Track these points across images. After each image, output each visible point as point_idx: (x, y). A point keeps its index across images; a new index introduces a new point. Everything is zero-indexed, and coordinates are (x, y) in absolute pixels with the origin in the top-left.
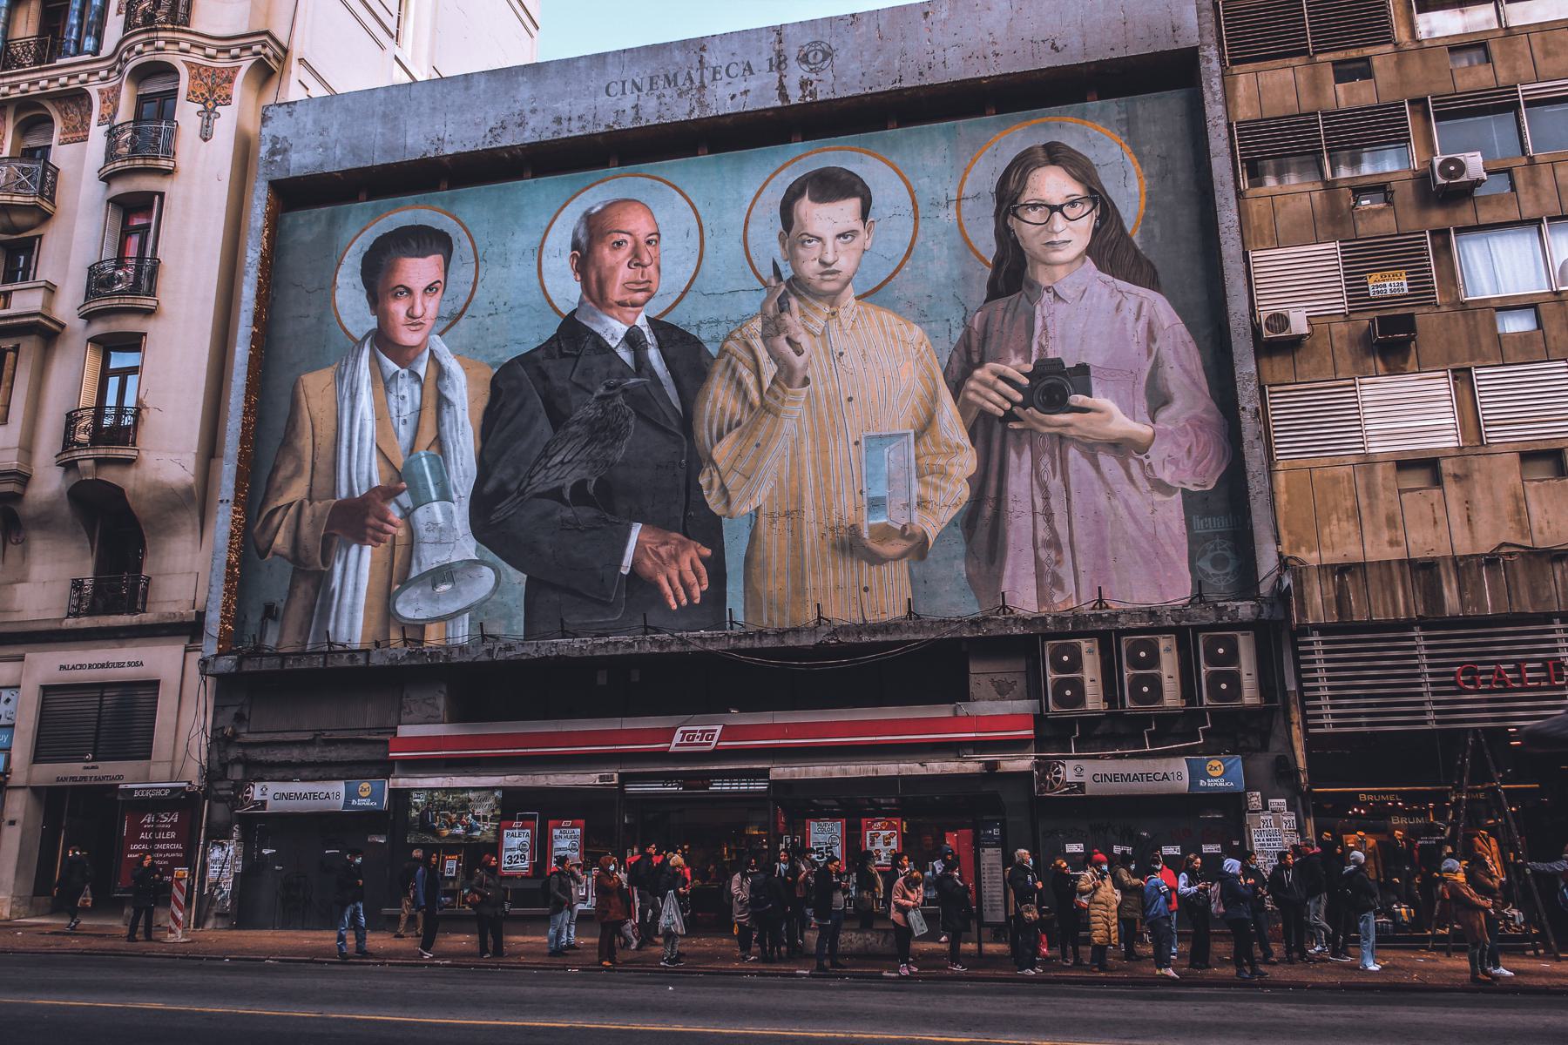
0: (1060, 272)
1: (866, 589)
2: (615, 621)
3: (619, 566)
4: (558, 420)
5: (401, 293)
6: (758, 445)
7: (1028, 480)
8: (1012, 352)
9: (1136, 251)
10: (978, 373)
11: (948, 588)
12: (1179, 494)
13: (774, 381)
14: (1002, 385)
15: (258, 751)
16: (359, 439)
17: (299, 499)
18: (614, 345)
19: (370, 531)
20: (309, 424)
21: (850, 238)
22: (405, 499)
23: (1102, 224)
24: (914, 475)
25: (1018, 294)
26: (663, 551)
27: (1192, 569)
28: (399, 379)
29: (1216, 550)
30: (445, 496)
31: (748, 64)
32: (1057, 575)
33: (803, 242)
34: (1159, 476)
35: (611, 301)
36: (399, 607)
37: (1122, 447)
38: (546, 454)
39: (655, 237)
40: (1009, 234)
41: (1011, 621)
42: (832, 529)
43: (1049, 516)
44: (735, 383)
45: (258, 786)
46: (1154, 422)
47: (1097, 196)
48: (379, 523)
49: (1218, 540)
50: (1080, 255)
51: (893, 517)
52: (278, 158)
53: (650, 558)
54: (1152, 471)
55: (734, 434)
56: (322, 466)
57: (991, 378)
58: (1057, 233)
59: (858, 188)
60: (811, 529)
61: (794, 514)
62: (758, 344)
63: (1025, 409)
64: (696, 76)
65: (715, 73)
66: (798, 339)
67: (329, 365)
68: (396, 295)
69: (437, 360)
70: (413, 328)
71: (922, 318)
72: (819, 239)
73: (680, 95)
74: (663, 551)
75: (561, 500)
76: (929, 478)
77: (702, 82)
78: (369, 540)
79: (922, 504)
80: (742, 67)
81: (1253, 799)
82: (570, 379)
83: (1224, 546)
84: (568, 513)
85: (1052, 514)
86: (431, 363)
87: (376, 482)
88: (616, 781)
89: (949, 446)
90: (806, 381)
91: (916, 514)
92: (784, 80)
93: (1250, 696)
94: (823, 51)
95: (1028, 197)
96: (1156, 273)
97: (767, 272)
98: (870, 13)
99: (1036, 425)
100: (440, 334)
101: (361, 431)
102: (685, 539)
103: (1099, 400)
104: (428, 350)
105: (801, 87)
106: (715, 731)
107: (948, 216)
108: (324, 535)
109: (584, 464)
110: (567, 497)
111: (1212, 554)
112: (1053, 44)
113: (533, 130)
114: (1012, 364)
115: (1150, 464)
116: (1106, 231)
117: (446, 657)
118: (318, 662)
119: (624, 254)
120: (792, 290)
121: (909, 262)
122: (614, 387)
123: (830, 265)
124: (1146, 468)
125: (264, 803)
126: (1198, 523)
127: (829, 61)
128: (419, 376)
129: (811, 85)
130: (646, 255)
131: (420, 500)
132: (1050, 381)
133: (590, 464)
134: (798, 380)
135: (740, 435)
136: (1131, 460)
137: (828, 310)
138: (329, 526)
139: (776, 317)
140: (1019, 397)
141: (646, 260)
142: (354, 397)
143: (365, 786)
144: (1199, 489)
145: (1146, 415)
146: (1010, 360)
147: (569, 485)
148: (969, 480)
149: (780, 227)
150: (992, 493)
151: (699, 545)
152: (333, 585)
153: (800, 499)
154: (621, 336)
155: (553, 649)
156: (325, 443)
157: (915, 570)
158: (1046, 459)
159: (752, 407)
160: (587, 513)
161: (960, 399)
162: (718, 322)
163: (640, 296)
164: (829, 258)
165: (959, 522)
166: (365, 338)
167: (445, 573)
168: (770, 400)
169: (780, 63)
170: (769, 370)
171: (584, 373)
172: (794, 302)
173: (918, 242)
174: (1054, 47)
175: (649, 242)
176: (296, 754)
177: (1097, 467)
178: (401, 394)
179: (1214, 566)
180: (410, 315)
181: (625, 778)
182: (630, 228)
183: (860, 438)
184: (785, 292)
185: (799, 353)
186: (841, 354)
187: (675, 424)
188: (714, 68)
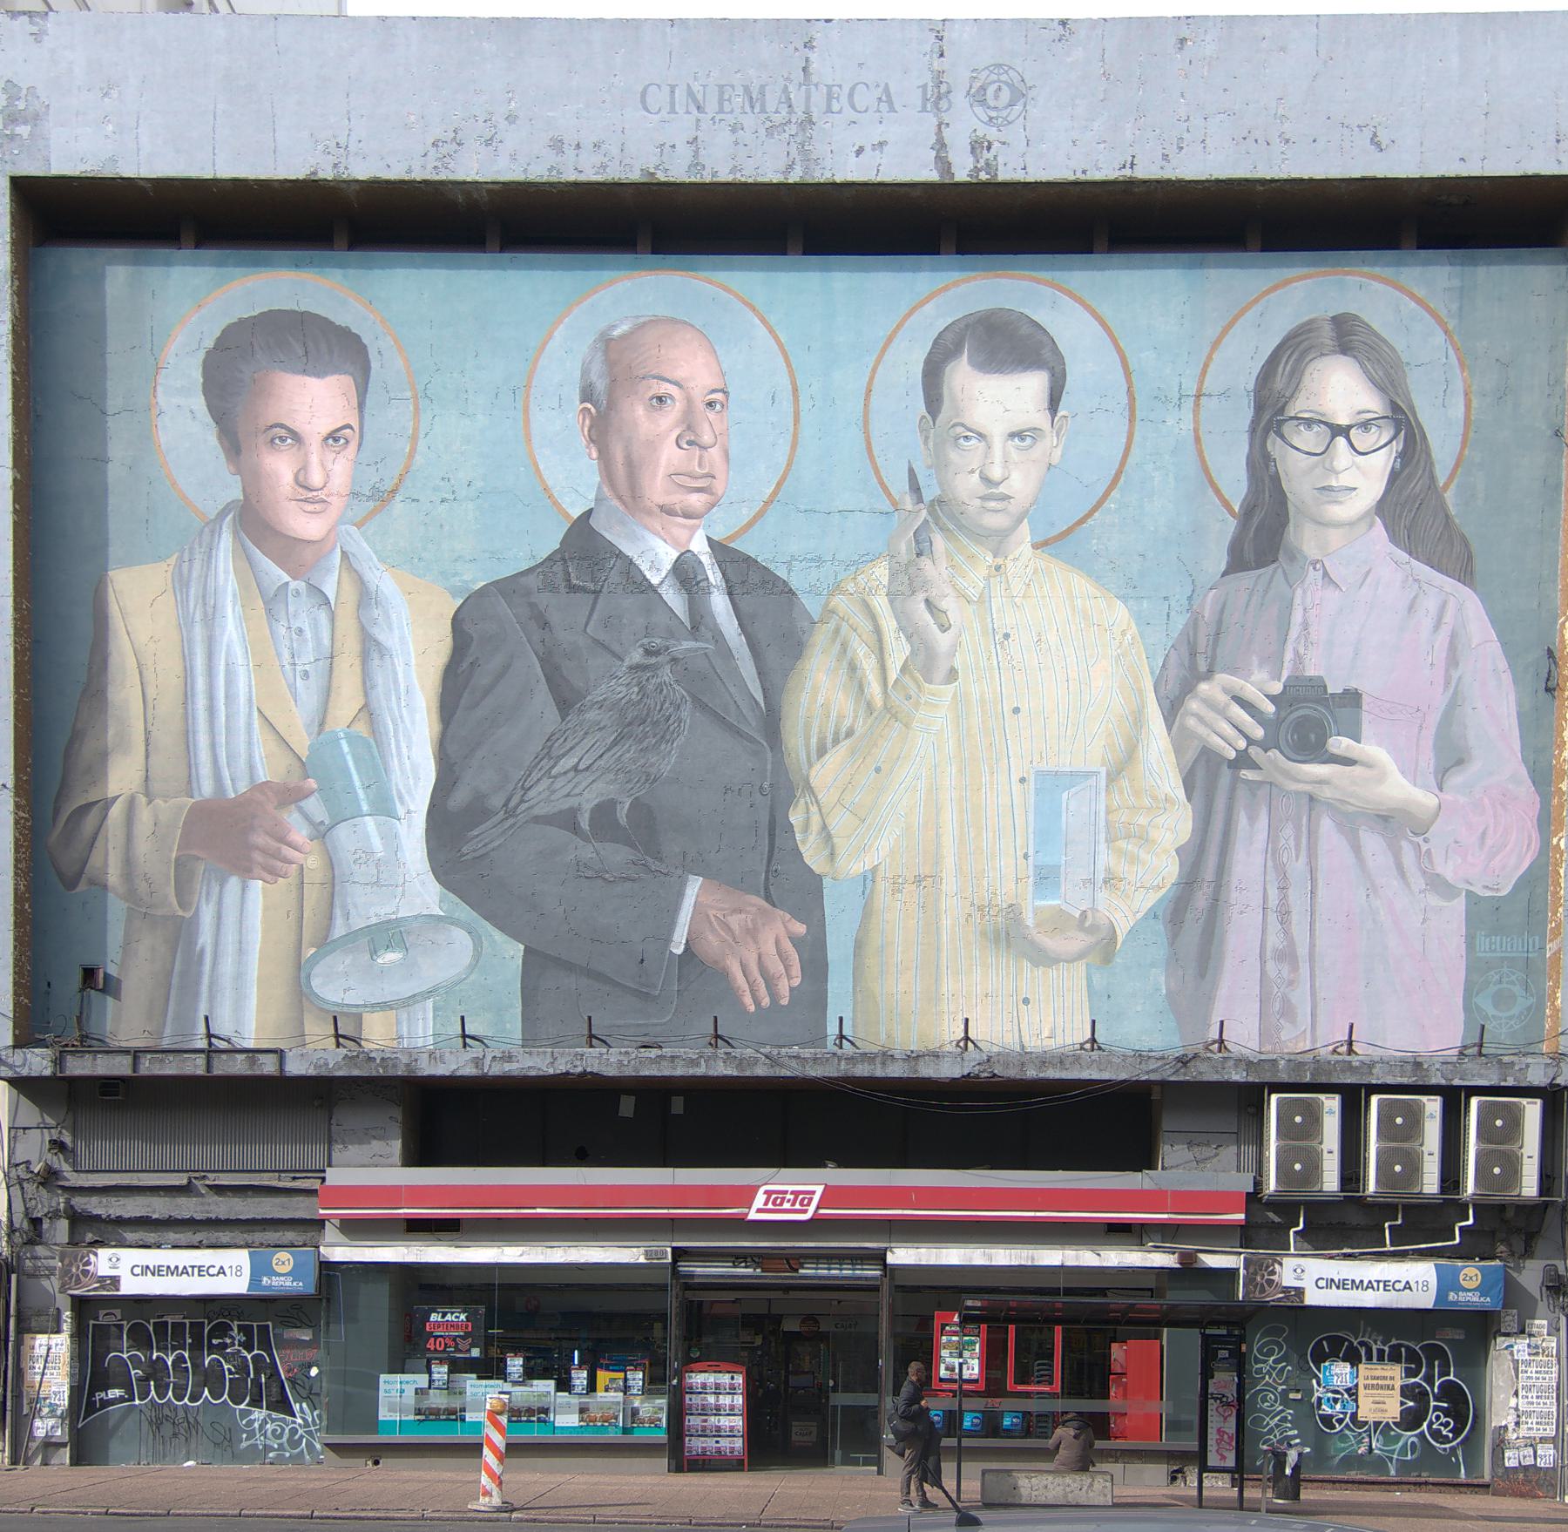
0: (1335, 537)
1: (1026, 1001)
2: (661, 1025)
3: (668, 940)
4: (566, 702)
5: (282, 439)
6: (878, 770)
7: (1259, 860)
8: (1255, 659)
9: (1447, 516)
10: (1203, 687)
11: (1139, 1009)
12: (1462, 898)
13: (904, 669)
14: (1237, 712)
15: (95, 1200)
16: (227, 697)
17: (127, 792)
18: (655, 581)
19: (258, 857)
20: (131, 662)
21: (1029, 441)
22: (313, 805)
23: (1403, 466)
24: (1102, 837)
25: (1274, 566)
26: (735, 921)
27: (1467, 1008)
28: (290, 598)
29: (1500, 982)
30: (384, 807)
31: (887, 90)
32: (1289, 1001)
33: (957, 439)
34: (1439, 870)
35: (649, 503)
36: (316, 983)
37: (1391, 821)
38: (548, 752)
39: (719, 396)
40: (1267, 466)
41: (1231, 1063)
42: (981, 908)
43: (1284, 914)
44: (845, 664)
45: (104, 1253)
46: (1441, 789)
47: (1402, 419)
48: (274, 844)
49: (1505, 970)
50: (1366, 515)
51: (1071, 898)
52: (23, 130)
53: (713, 930)
54: (1431, 862)
55: (845, 745)
56: (166, 738)
57: (1223, 698)
58: (1337, 473)
59: (1046, 353)
60: (952, 910)
61: (926, 880)
62: (881, 603)
63: (1266, 751)
64: (797, 97)
65: (830, 97)
66: (943, 605)
67: (160, 559)
68: (272, 441)
69: (356, 571)
70: (310, 508)
71: (1130, 591)
72: (981, 436)
73: (770, 132)
74: (735, 921)
75: (575, 829)
76: (1122, 844)
77: (807, 113)
78: (257, 870)
79: (1111, 880)
80: (878, 92)
81: (1508, 1318)
82: (585, 631)
83: (1513, 978)
84: (587, 852)
85: (1288, 912)
86: (345, 575)
87: (262, 776)
88: (669, 1260)
89: (1155, 798)
90: (952, 675)
91: (1102, 895)
92: (946, 133)
93: (1529, 1186)
94: (1011, 86)
95: (1298, 407)
96: (1470, 558)
97: (900, 486)
98: (1093, 24)
99: (1280, 779)
100: (359, 525)
101: (229, 682)
102: (766, 905)
103: (1370, 748)
104: (338, 550)
105: (973, 151)
106: (813, 1193)
107: (1180, 423)
108: (177, 859)
109: (612, 776)
110: (584, 823)
111: (1496, 988)
112: (1375, 135)
113: (513, 158)
114: (1253, 678)
115: (1428, 852)
116: (1409, 478)
117: (408, 1065)
118: (196, 1066)
119: (669, 419)
120: (937, 522)
121: (1115, 494)
122: (657, 653)
123: (998, 484)
124: (1423, 856)
125: (115, 1281)
126: (1482, 942)
127: (1019, 107)
128: (327, 599)
129: (989, 148)
130: (706, 427)
131: (342, 813)
132: (1301, 712)
133: (621, 776)
134: (941, 672)
135: (853, 752)
136: (1404, 843)
137: (990, 558)
138: (185, 842)
139: (910, 563)
140: (1259, 733)
141: (707, 438)
142: (211, 619)
143: (283, 1260)
144: (1489, 894)
145: (1432, 777)
146: (1250, 673)
147: (588, 807)
148: (1177, 851)
149: (922, 409)
150: (1209, 873)
151: (788, 916)
152: (201, 941)
153: (937, 860)
154: (667, 566)
155: (578, 1063)
156: (167, 705)
157: (1096, 979)
158: (1288, 831)
159: (870, 707)
160: (617, 855)
161: (1175, 728)
162: (819, 560)
163: (696, 500)
164: (996, 473)
165: (1160, 913)
166: (222, 515)
167: (388, 934)
168: (896, 698)
169: (939, 98)
170: (898, 651)
171: (606, 624)
172: (939, 542)
173: (1131, 460)
174: (1375, 141)
175: (710, 404)
176: (159, 1207)
177: (1356, 848)
178: (296, 624)
179: (1496, 1005)
180: (301, 483)
181: (679, 1253)
182: (680, 374)
183: (1028, 772)
184: (926, 521)
185: (944, 628)
186: (1007, 636)
187: (754, 724)
188: (829, 87)
